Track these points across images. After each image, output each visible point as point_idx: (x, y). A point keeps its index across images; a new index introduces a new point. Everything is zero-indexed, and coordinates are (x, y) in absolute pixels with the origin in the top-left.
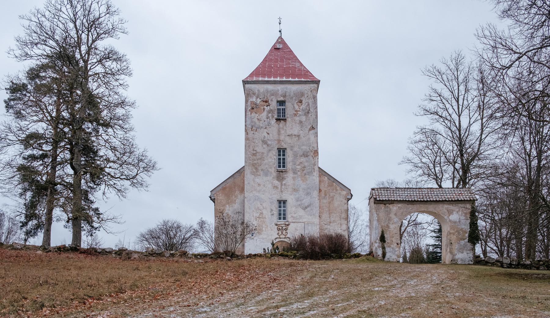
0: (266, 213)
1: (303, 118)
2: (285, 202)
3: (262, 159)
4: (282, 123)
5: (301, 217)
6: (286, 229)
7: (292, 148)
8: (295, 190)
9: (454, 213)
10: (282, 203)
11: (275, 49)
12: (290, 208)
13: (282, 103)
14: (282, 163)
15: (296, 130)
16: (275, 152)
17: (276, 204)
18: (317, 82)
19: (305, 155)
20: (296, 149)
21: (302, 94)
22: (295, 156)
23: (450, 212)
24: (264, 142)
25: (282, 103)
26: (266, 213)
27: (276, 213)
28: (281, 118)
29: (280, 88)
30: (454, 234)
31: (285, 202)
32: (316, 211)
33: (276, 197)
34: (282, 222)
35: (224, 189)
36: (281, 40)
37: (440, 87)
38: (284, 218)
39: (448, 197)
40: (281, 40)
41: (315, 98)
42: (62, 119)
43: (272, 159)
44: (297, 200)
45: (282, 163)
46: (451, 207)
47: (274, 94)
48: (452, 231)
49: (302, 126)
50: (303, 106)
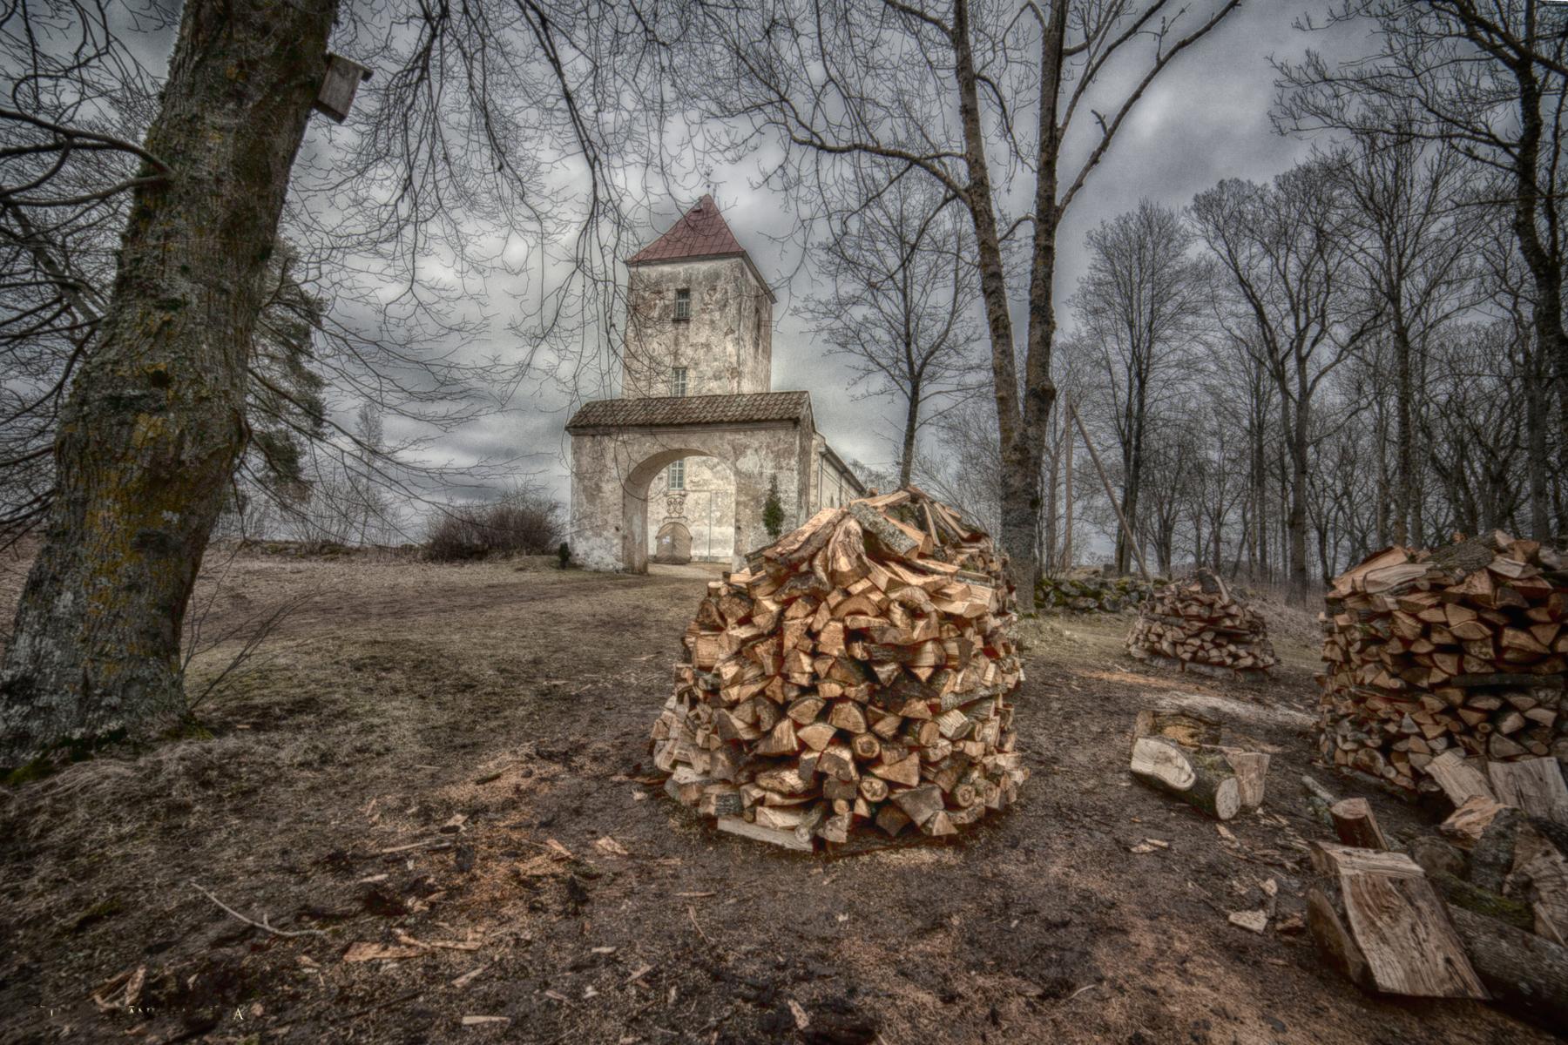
1: (717, 315)
4: (682, 326)
5: (706, 482)
6: (681, 503)
9: (749, 452)
20: (703, 367)
25: (684, 293)
29: (681, 269)
30: (746, 506)
38: (680, 485)
42: (69, 306)
47: (673, 278)
48: (743, 498)
49: (714, 329)
50: (718, 296)
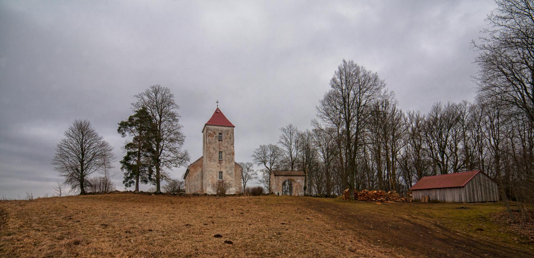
0: (215, 177)
2: (222, 172)
3: (213, 155)
4: (221, 142)
7: (225, 151)
8: (226, 168)
10: (221, 173)
11: (216, 112)
12: (224, 175)
13: (220, 134)
14: (220, 157)
15: (226, 145)
16: (218, 153)
17: (218, 173)
18: (234, 127)
19: (230, 154)
21: (228, 131)
22: (226, 154)
23: (297, 179)
24: (214, 149)
26: (215, 177)
27: (218, 176)
28: (220, 140)
29: (220, 128)
31: (222, 172)
32: (234, 176)
33: (218, 170)
34: (221, 180)
35: (193, 166)
36: (218, 109)
37: (285, 134)
39: (296, 174)
40: (218, 109)
41: (233, 133)
43: (217, 155)
44: (227, 171)
45: (220, 157)
46: (297, 177)
47: (218, 130)
50: (229, 136)
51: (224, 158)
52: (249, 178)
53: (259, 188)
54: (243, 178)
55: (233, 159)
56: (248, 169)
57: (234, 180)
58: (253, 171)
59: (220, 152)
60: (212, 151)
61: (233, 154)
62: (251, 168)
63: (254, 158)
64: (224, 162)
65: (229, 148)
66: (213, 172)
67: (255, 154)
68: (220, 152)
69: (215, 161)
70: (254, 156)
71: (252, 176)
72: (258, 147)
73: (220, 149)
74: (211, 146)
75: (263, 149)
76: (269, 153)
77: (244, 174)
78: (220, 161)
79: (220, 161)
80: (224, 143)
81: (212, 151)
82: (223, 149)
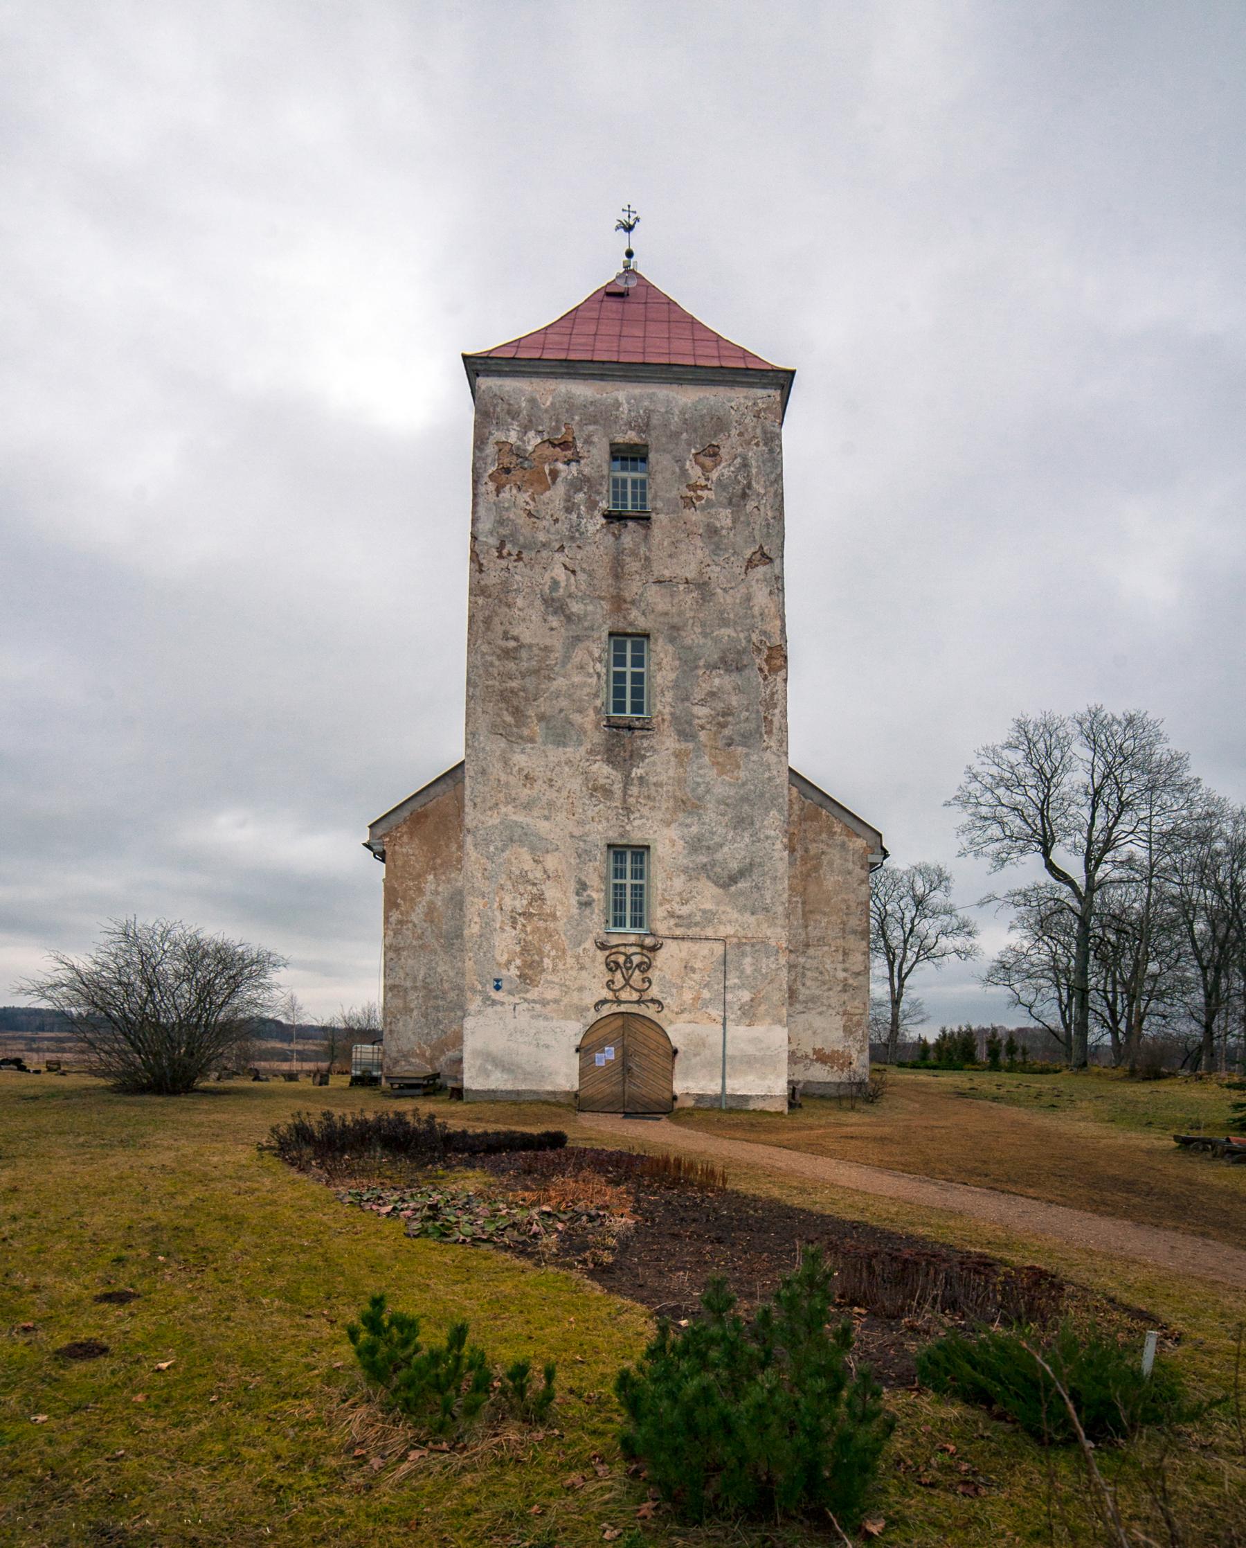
0: (561, 899)
2: (641, 852)
3: (542, 672)
4: (630, 535)
8: (688, 805)
10: (629, 856)
13: (630, 455)
16: (598, 646)
17: (600, 862)
19: (731, 662)
21: (720, 424)
22: (688, 663)
24: (554, 605)
26: (561, 899)
31: (641, 852)
32: (777, 891)
33: (601, 831)
43: (585, 677)
44: (695, 845)
47: (601, 416)
50: (722, 471)
51: (661, 705)
52: (926, 952)
53: (560, 1133)
54: (889, 951)
55: (768, 720)
56: (919, 902)
57: (777, 935)
58: (949, 912)
59: (628, 643)
60: (532, 626)
61: (777, 658)
62: (937, 898)
63: (964, 818)
64: (667, 742)
65: (727, 600)
66: (539, 847)
67: (975, 787)
68: (628, 643)
69: (560, 733)
70: (964, 800)
71: (944, 942)
72: (1002, 733)
73: (618, 603)
74: (521, 576)
75: (1039, 748)
76: (1076, 779)
77: (896, 935)
78: (625, 728)
79: (625, 728)
80: (672, 549)
81: (532, 626)
82: (651, 606)
